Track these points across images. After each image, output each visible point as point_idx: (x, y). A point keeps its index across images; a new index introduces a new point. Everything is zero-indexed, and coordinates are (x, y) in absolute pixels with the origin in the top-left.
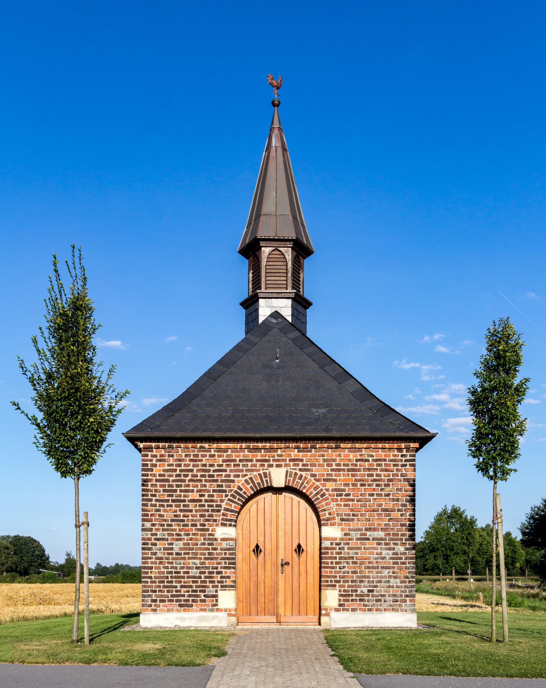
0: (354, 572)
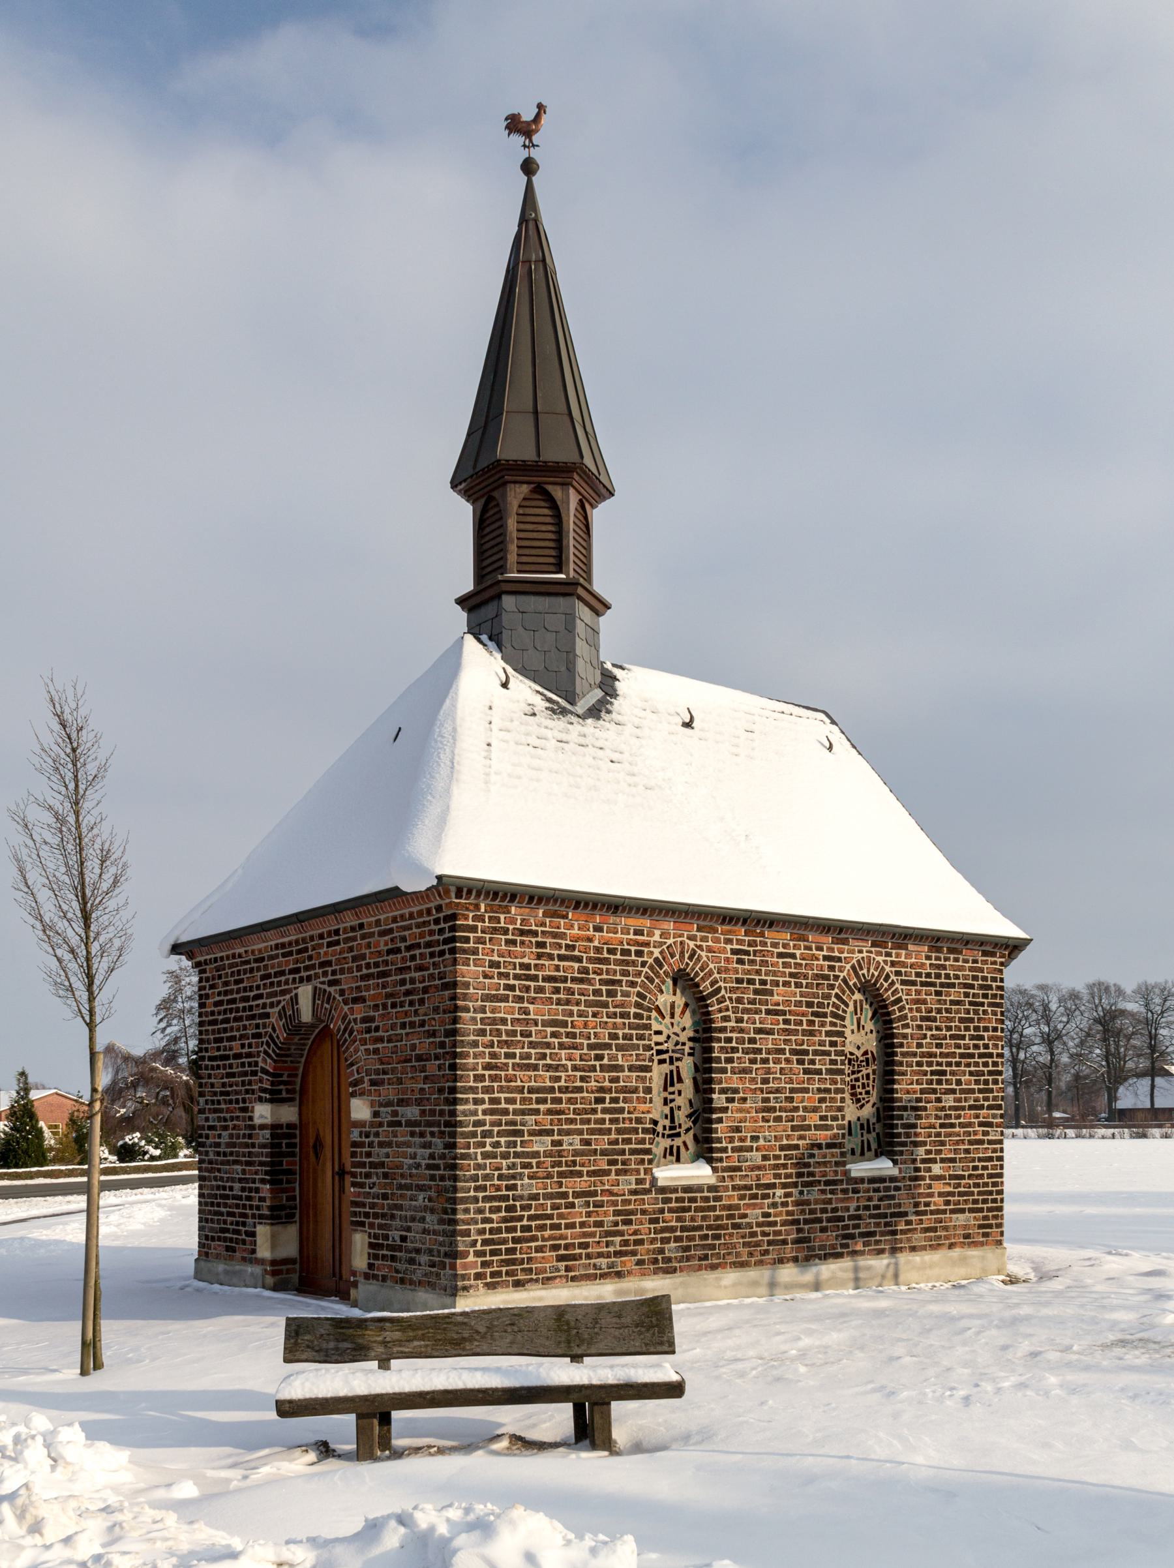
0: (385, 1197)
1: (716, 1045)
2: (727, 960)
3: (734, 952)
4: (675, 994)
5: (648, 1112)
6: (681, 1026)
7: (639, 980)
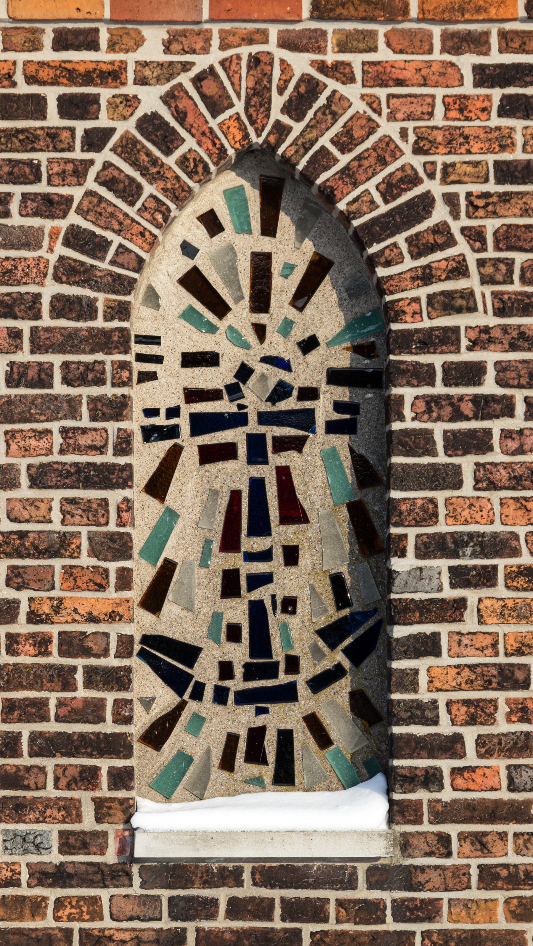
1: (408, 393)
2: (460, 105)
3: (485, 76)
4: (269, 228)
5: (113, 617)
6: (299, 334)
7: (77, 193)
